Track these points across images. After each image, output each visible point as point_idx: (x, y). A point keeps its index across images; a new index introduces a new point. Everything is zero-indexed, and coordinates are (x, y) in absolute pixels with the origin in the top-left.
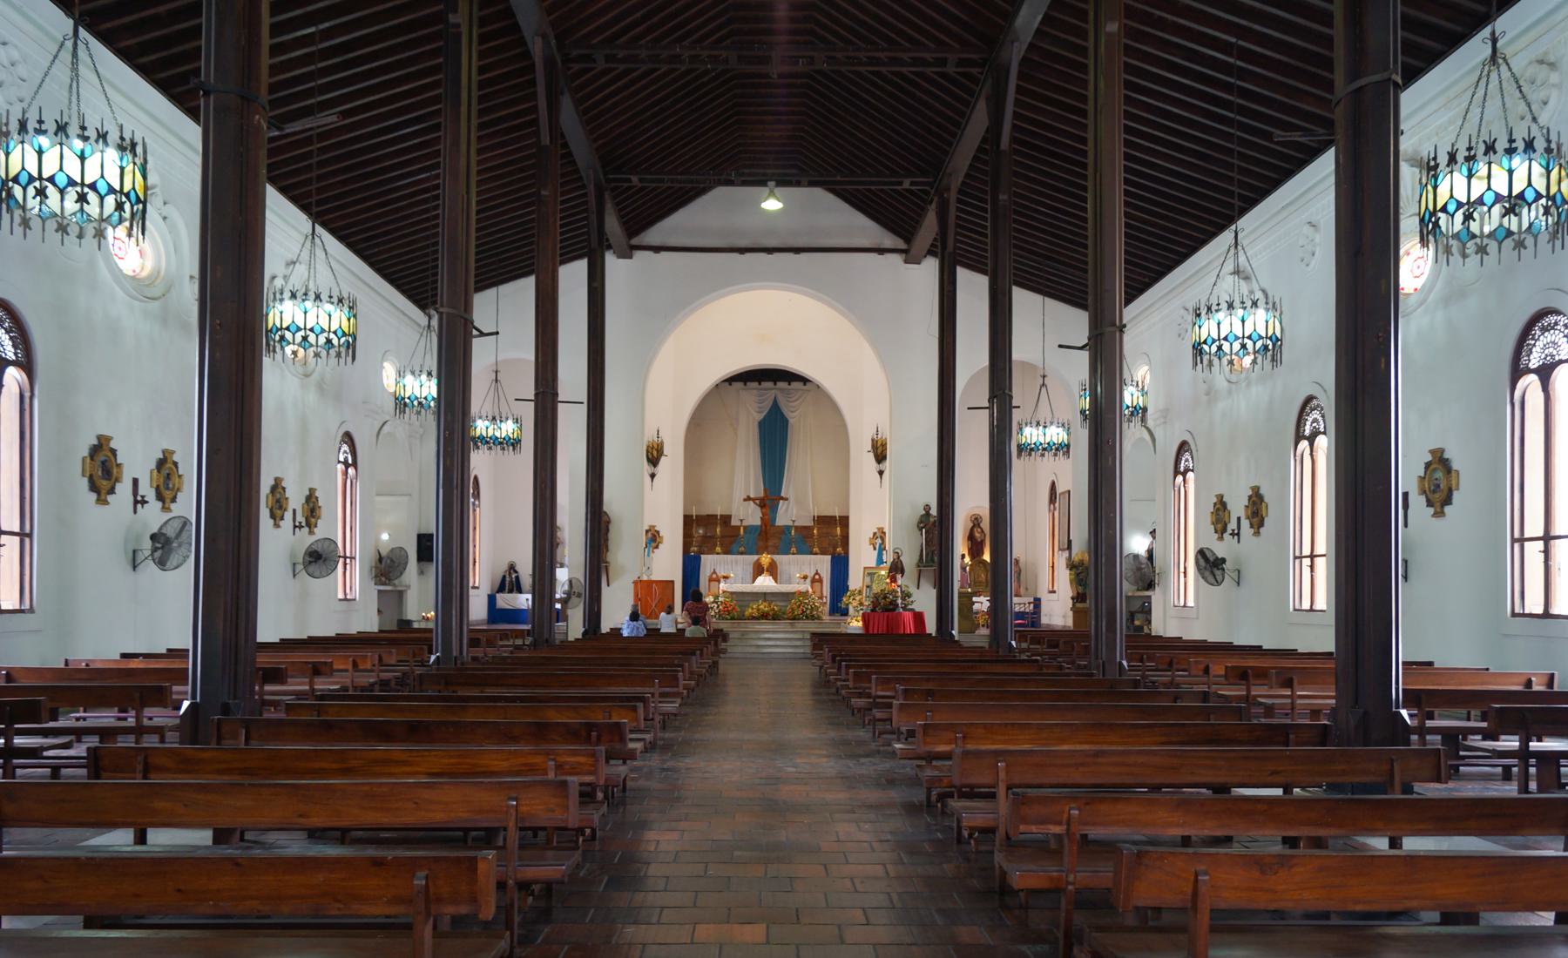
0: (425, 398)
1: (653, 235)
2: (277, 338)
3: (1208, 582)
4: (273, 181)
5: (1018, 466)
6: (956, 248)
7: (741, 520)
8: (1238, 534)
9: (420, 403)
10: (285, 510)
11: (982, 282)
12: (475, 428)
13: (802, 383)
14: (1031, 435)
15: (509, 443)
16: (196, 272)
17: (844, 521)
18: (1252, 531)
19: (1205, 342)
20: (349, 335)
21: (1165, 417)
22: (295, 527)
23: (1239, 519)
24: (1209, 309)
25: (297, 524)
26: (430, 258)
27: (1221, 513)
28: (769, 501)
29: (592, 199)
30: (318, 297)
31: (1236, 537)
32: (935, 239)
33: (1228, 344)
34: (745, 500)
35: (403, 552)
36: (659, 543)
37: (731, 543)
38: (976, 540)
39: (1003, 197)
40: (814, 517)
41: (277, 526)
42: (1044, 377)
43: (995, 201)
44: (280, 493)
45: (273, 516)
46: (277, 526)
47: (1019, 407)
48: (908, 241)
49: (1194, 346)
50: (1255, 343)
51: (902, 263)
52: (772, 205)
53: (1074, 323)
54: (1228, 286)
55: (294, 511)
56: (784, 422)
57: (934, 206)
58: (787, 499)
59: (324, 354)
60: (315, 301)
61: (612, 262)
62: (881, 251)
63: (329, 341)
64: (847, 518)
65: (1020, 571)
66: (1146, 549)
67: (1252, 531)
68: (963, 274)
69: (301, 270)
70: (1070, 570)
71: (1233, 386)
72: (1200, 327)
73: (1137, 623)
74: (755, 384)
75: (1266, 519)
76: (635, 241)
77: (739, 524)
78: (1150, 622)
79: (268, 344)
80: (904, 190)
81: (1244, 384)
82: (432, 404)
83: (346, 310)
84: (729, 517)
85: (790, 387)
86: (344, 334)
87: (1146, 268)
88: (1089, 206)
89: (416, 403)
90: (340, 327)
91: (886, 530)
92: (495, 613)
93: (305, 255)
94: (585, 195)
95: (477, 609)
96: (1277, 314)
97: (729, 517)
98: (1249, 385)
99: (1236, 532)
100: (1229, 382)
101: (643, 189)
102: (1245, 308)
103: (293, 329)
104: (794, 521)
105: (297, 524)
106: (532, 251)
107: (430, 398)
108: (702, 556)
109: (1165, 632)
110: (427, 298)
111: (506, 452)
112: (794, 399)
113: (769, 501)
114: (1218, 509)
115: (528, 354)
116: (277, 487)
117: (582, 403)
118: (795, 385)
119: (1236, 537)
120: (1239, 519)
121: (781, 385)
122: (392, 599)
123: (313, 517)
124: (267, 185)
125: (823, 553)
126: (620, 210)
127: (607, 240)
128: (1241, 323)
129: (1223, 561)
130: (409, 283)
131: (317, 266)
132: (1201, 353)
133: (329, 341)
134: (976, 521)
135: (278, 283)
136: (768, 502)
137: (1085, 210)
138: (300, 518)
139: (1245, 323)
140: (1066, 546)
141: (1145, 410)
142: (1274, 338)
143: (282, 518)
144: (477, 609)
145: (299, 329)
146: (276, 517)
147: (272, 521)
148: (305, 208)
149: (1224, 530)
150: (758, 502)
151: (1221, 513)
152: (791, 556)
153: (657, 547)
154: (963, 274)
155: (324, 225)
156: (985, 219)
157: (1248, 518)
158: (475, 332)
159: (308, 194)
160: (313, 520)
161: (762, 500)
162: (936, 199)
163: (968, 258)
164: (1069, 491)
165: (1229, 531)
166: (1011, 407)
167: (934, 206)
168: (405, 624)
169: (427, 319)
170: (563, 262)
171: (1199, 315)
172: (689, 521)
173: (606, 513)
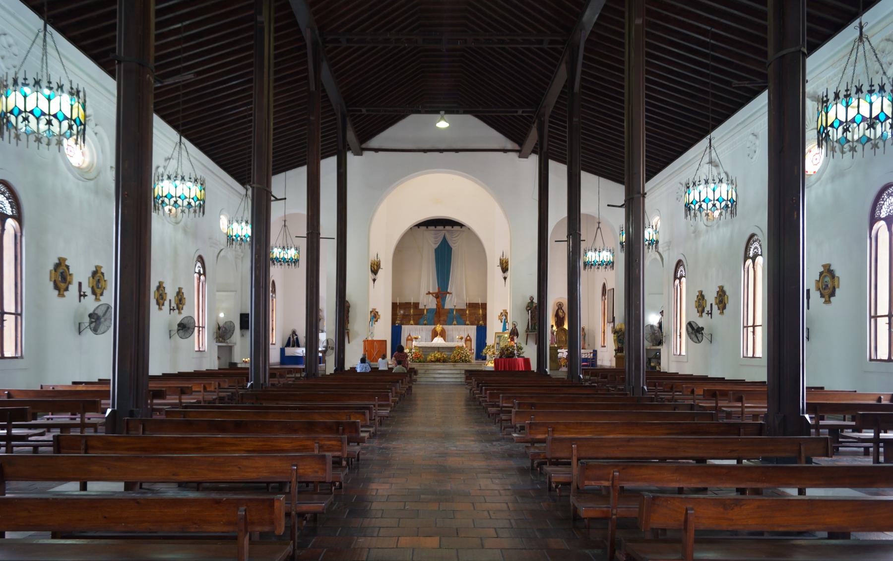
0: (244, 236)
1: (375, 142)
2: (160, 202)
4: (158, 112)
5: (584, 275)
7: (425, 306)
8: (711, 314)
9: (241, 239)
10: (165, 300)
11: (563, 168)
14: (592, 256)
17: (484, 306)
18: (719, 311)
19: (692, 203)
20: (201, 200)
21: (669, 246)
22: (171, 309)
23: (711, 305)
24: (694, 184)
27: (701, 301)
28: (441, 294)
30: (183, 178)
32: (536, 144)
34: (427, 294)
36: (378, 318)
38: (560, 317)
40: (467, 304)
41: (160, 309)
42: (599, 223)
45: (158, 303)
46: (160, 309)
48: (521, 145)
49: (685, 205)
52: (443, 124)
53: (617, 192)
54: (706, 170)
55: (170, 300)
56: (450, 249)
57: (535, 125)
60: (181, 180)
61: (351, 158)
62: (505, 151)
63: (189, 203)
67: (719, 311)
68: (552, 164)
70: (614, 334)
71: (709, 228)
72: (689, 194)
73: (652, 364)
77: (423, 307)
78: (660, 364)
79: (155, 206)
81: (715, 227)
83: (199, 185)
84: (418, 304)
86: (198, 200)
87: (658, 160)
88: (625, 124)
89: (239, 239)
91: (508, 311)
92: (284, 359)
93: (176, 154)
94: (335, 119)
95: (274, 357)
97: (418, 304)
98: (718, 227)
100: (706, 226)
102: (715, 183)
105: (172, 308)
111: (290, 267)
113: (441, 294)
114: (699, 299)
116: (160, 287)
117: (334, 239)
118: (457, 228)
119: (710, 315)
120: (711, 305)
123: (181, 304)
125: (472, 324)
127: (348, 145)
129: (702, 329)
132: (689, 210)
134: (560, 306)
135: (161, 170)
138: (173, 305)
140: (612, 320)
141: (657, 242)
143: (163, 305)
144: (274, 357)
146: (160, 303)
147: (157, 307)
148: (175, 127)
149: (703, 311)
150: (434, 295)
151: (701, 301)
152: (453, 326)
153: (377, 321)
154: (552, 164)
155: (186, 137)
160: (181, 306)
162: (537, 121)
164: (613, 289)
165: (706, 311)
166: (580, 241)
167: (535, 125)
168: (233, 365)
169: (245, 190)
170: (323, 158)
171: (688, 187)
172: (395, 306)
173: (347, 302)
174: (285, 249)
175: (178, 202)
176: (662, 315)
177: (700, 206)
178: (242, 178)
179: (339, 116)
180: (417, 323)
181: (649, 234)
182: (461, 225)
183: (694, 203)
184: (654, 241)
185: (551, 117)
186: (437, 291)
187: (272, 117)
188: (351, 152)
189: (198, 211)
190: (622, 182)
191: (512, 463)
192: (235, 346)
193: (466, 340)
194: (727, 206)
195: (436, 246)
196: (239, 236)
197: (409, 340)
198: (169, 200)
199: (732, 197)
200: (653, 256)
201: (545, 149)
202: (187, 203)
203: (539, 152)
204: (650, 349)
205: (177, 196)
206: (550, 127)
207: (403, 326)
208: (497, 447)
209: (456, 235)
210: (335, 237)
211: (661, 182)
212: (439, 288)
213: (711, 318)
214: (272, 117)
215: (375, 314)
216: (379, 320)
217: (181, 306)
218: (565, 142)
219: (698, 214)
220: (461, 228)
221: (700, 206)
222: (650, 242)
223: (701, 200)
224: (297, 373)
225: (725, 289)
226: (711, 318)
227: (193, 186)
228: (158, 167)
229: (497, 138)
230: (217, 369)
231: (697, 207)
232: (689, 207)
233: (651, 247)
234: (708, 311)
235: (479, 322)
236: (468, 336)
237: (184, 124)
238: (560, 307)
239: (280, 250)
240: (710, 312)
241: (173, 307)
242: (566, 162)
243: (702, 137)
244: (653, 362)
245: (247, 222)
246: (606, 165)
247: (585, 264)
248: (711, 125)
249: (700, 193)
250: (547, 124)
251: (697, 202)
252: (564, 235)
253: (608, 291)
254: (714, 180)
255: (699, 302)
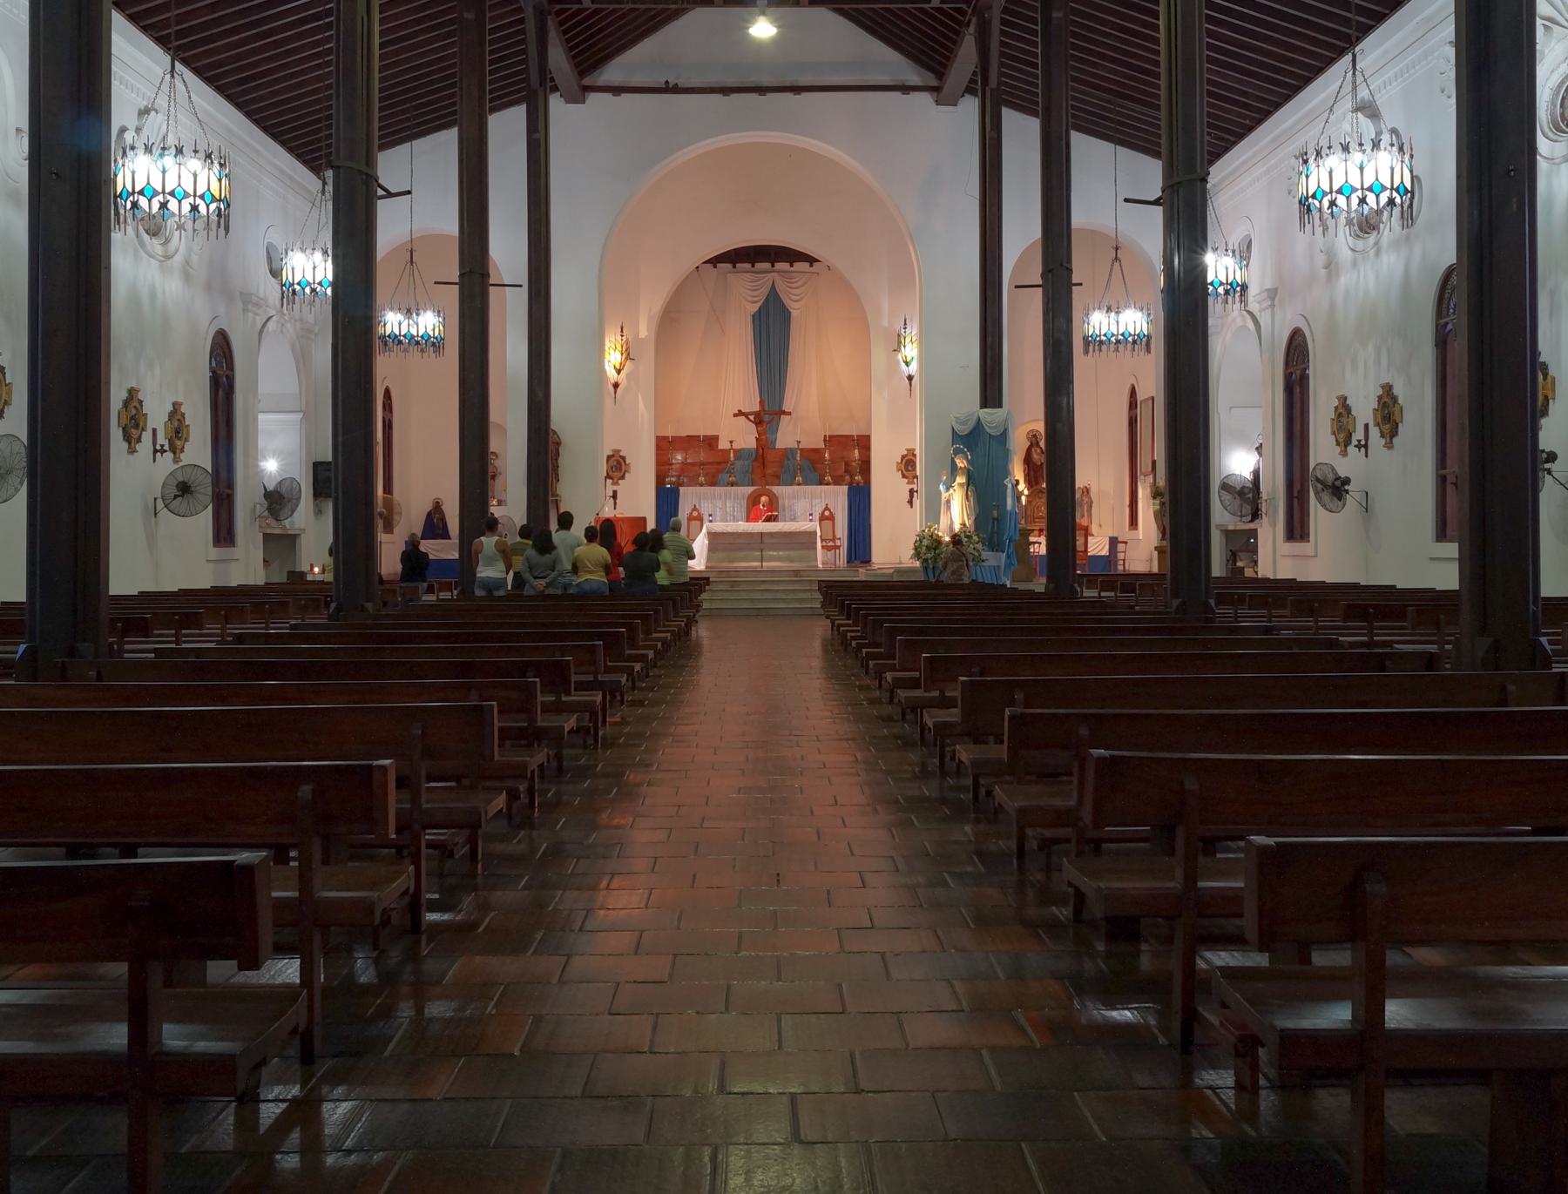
0: (320, 284)
1: (612, 73)
2: (129, 205)
3: (1327, 509)
4: (119, 5)
5: (1082, 364)
6: (999, 83)
7: (731, 442)
8: (1366, 446)
9: (313, 290)
10: (143, 430)
11: (1033, 125)
12: (385, 325)
13: (807, 264)
14: (1099, 323)
15: (429, 344)
16: (25, 124)
17: (864, 443)
18: (1383, 441)
19: (1314, 196)
20: (220, 200)
21: (1273, 299)
22: (155, 451)
23: (1366, 426)
24: (1319, 154)
25: (158, 447)
26: (322, 153)
27: (1343, 420)
28: (767, 417)
29: (531, 26)
30: (179, 151)
31: (1363, 449)
32: (974, 73)
33: (1344, 199)
34: (735, 415)
35: (295, 484)
36: (625, 471)
37: (719, 471)
38: (1035, 464)
39: (1057, 14)
40: (825, 436)
41: (132, 451)
42: (1117, 249)
43: (1047, 21)
44: (135, 407)
45: (127, 438)
46: (132, 451)
47: (1081, 284)
48: (940, 76)
49: (1300, 202)
50: (1377, 196)
51: (934, 104)
52: (763, 29)
53: (1149, 174)
54: (1347, 123)
55: (154, 431)
56: (785, 315)
57: (972, 29)
58: (790, 414)
59: (189, 225)
60: (176, 156)
61: (556, 103)
62: (906, 89)
63: (194, 208)
64: (868, 438)
65: (1092, 502)
66: (1252, 469)
67: (1383, 441)
68: (1008, 115)
69: (156, 121)
70: (1154, 498)
71: (1359, 257)
72: (1307, 177)
73: (1239, 564)
74: (747, 266)
75: (1400, 425)
76: (587, 81)
77: (727, 446)
78: (1256, 562)
79: (117, 213)
80: (932, 8)
81: (1372, 252)
82: (329, 291)
83: (216, 167)
84: (715, 439)
85: (792, 269)
86: (214, 199)
87: (1246, 106)
88: (1162, 23)
89: (308, 290)
90: (209, 189)
91: (917, 452)
92: (414, 561)
93: (162, 102)
94: (522, 21)
95: (390, 561)
96: (1407, 157)
97: (715, 439)
98: (1378, 253)
99: (1363, 443)
100: (1353, 250)
101: (597, 11)
102: (1364, 151)
103: (148, 193)
104: (799, 442)
105: (158, 447)
106: (453, 95)
107: (325, 284)
108: (680, 488)
109: (1275, 572)
110: (320, 158)
111: (425, 355)
112: (800, 283)
113: (767, 417)
114: (1340, 415)
115: (449, 225)
116: (132, 397)
117: (521, 286)
118: (801, 266)
119: (1363, 449)
120: (1366, 426)
121: (780, 266)
122: (281, 544)
123: (179, 439)
124: (113, 11)
125: (837, 481)
126: (568, 41)
127: (552, 79)
128: (1359, 171)
129: (1347, 481)
130: (297, 138)
131: (179, 116)
132: (1309, 210)
133: (194, 208)
134: (1033, 439)
135: (129, 137)
136: (767, 418)
137: (1156, 28)
138: (162, 440)
139: (1365, 170)
140: (1150, 469)
141: (1244, 287)
142: (1402, 190)
143: (139, 440)
144: (390, 561)
145: (156, 193)
146: (131, 440)
147: (126, 445)
148: (162, 41)
149: (1347, 442)
150: (752, 417)
151: (1343, 420)
152: (796, 487)
153: (623, 477)
154: (1008, 115)
155: (185, 62)
156: (1035, 44)
157: (1377, 424)
158: (380, 192)
159: (166, 24)
160: (178, 443)
161: (757, 414)
162: (974, 20)
163: (1018, 97)
164: (1153, 398)
165: (1354, 442)
166: (1070, 285)
167: (972, 29)
168: (297, 577)
169: (320, 182)
170: (493, 110)
171: (1306, 162)
172: (664, 446)
173: (555, 432)
174: (411, 314)
175: (169, 206)
176: (1260, 454)
177: (1333, 203)
178: (309, 152)
179: (529, 14)
180: (713, 483)
181: (1227, 269)
182: (811, 260)
183: (1319, 196)
184: (1238, 285)
185: (1005, 10)
186: (756, 408)
187: (376, 17)
188: (559, 94)
189: (214, 226)
190: (1034, 114)
191: (835, 703)
192: (302, 536)
193: (822, 518)
194: (1391, 202)
195: (755, 308)
196: (309, 284)
197: (695, 519)
198: (150, 200)
199: (1402, 182)
200: (1239, 322)
201: (993, 83)
202: (189, 208)
203: (1164, 150)
204: (1234, 532)
205: (167, 191)
206: (1003, 33)
207: (682, 489)
208: (929, 789)
209: (800, 283)
210: (524, 281)
211: (1253, 156)
212: (762, 403)
213: (1367, 456)
214: (376, 17)
215: (619, 463)
216: (627, 475)
217: (178, 443)
218: (1035, 66)
219: (1331, 223)
220: (811, 266)
221: (1333, 203)
222: (1229, 287)
223: (1335, 189)
224: (440, 590)
225: (1397, 391)
226: (1367, 456)
227: (203, 168)
228: (123, 130)
229: (890, 62)
230: (263, 583)
231: (1326, 203)
232: (1309, 206)
233: (1230, 298)
234: (1359, 441)
235: (852, 477)
236: (827, 508)
237: (180, 34)
238: (1034, 442)
239: (400, 317)
240: (1363, 443)
241: (162, 446)
242: (1160, 153)
243: (1341, 52)
244: (1241, 560)
245: (325, 252)
246: (1129, 117)
247: (1087, 342)
248: (1354, 23)
249: (1330, 173)
250: (996, 27)
251: (1325, 194)
252: (1035, 275)
253: (1141, 402)
254: (1361, 145)
255: (1340, 422)
